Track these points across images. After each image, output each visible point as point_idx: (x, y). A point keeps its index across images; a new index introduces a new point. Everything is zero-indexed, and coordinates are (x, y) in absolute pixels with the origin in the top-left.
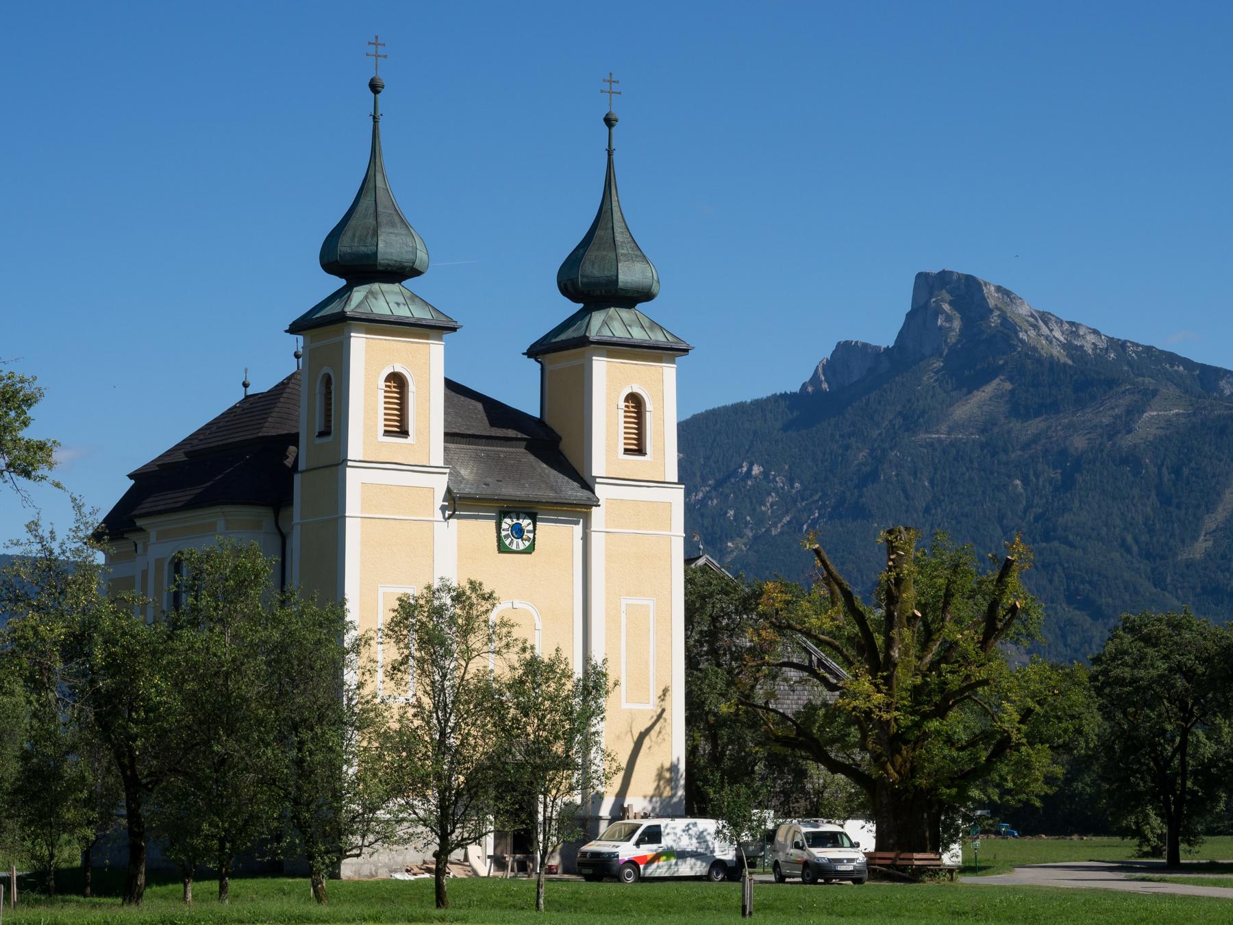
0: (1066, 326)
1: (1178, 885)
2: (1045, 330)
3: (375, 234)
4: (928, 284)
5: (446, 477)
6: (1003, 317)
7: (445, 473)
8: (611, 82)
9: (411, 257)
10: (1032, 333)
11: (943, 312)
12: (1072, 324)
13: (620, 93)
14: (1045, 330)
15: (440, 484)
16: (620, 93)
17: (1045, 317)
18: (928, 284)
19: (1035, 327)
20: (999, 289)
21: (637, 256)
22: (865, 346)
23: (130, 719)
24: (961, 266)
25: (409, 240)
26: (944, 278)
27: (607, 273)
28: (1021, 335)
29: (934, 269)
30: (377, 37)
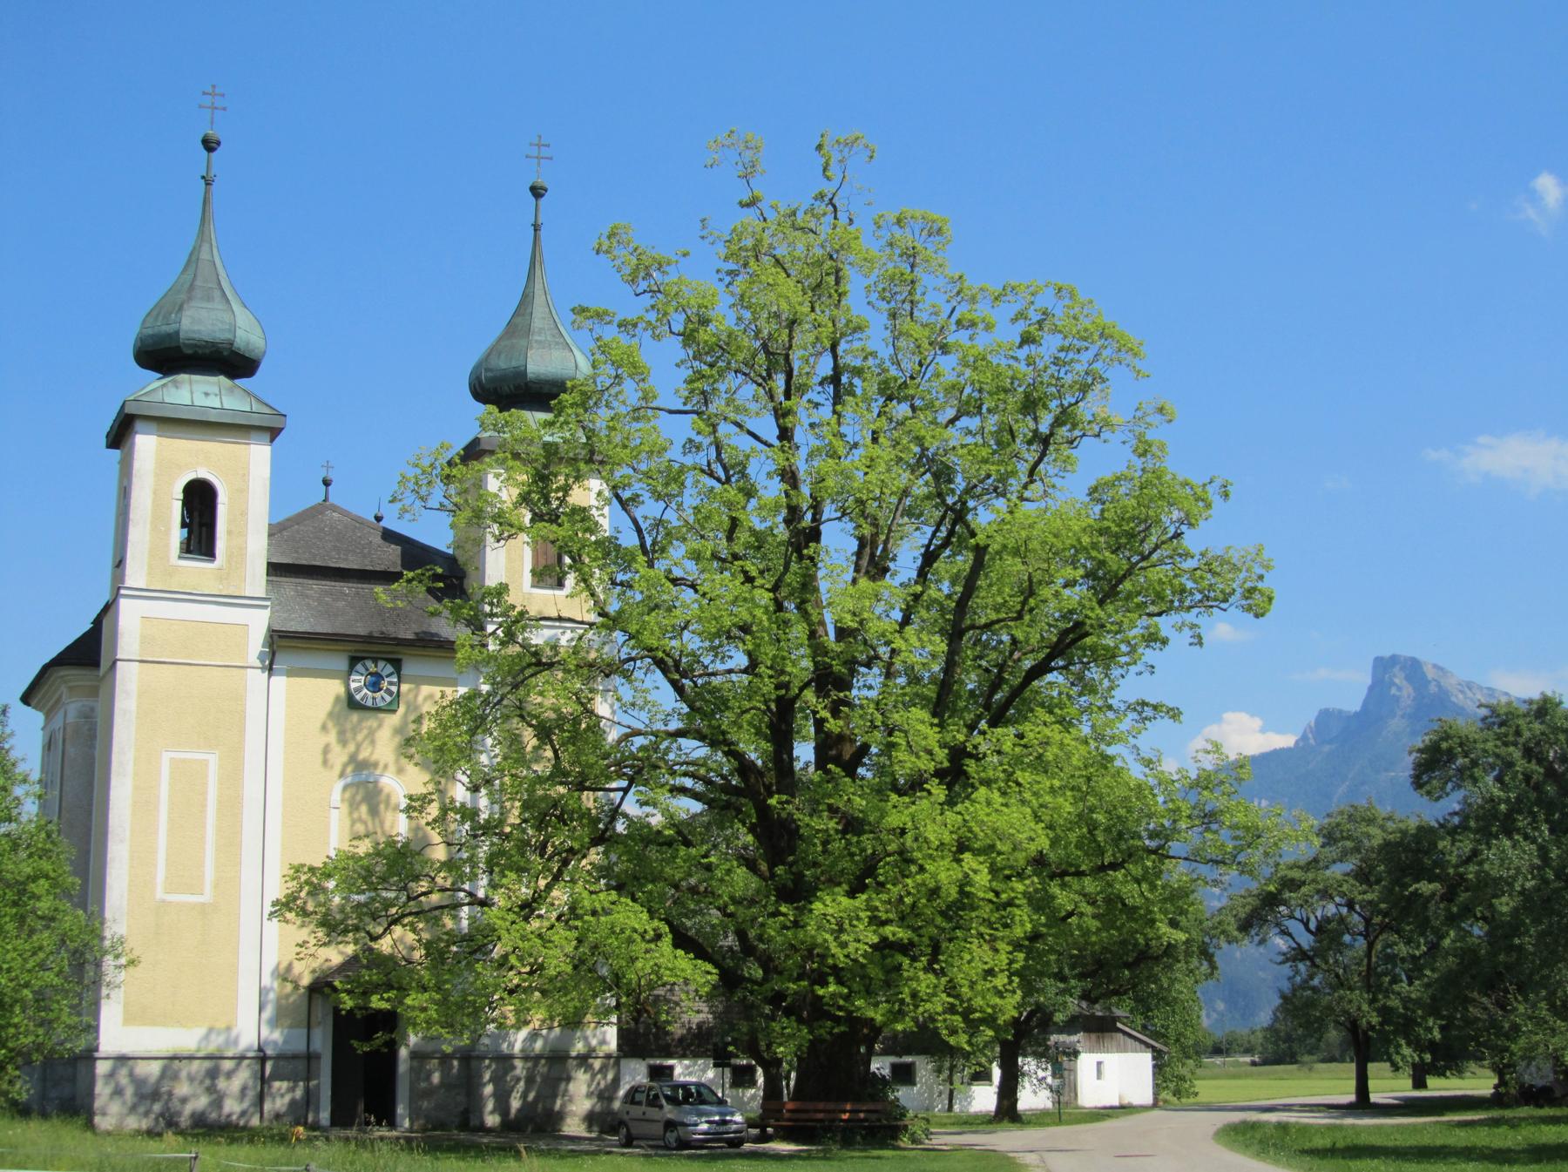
0: (1485, 691)
1: (1326, 1102)
2: (1469, 694)
3: (181, 308)
4: (1383, 666)
5: (266, 613)
6: (1439, 686)
7: (265, 607)
8: (539, 146)
9: (228, 336)
10: (1461, 696)
11: (1395, 684)
12: (1489, 689)
13: (551, 159)
14: (1469, 694)
15: (258, 623)
16: (551, 159)
17: (1469, 686)
18: (1383, 666)
19: (1462, 692)
20: (1435, 666)
21: (557, 343)
22: (1340, 712)
23: (472, 983)
24: (1405, 651)
25: (227, 317)
26: (1394, 659)
27: (514, 364)
28: (1453, 699)
29: (1387, 653)
30: (214, 87)
